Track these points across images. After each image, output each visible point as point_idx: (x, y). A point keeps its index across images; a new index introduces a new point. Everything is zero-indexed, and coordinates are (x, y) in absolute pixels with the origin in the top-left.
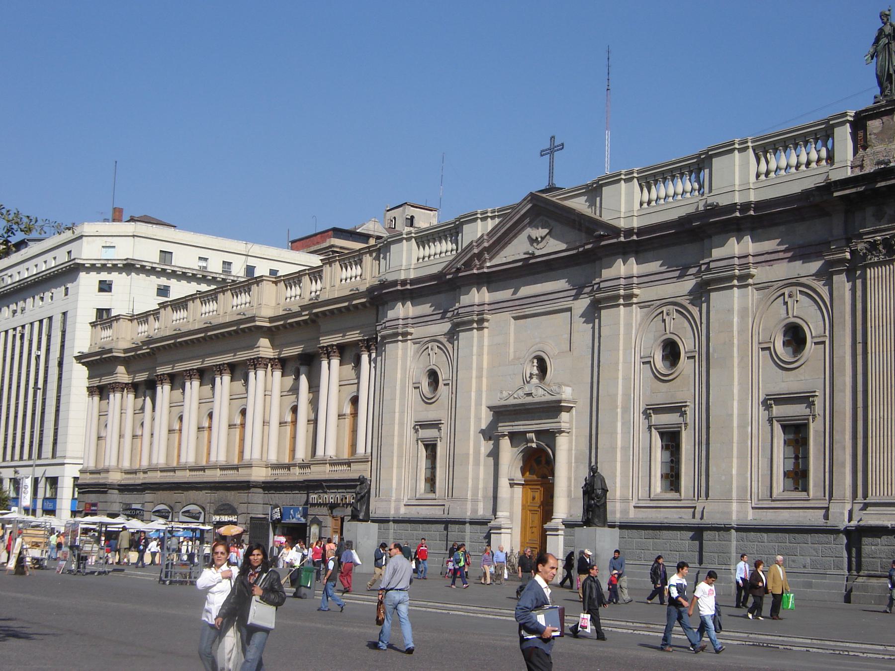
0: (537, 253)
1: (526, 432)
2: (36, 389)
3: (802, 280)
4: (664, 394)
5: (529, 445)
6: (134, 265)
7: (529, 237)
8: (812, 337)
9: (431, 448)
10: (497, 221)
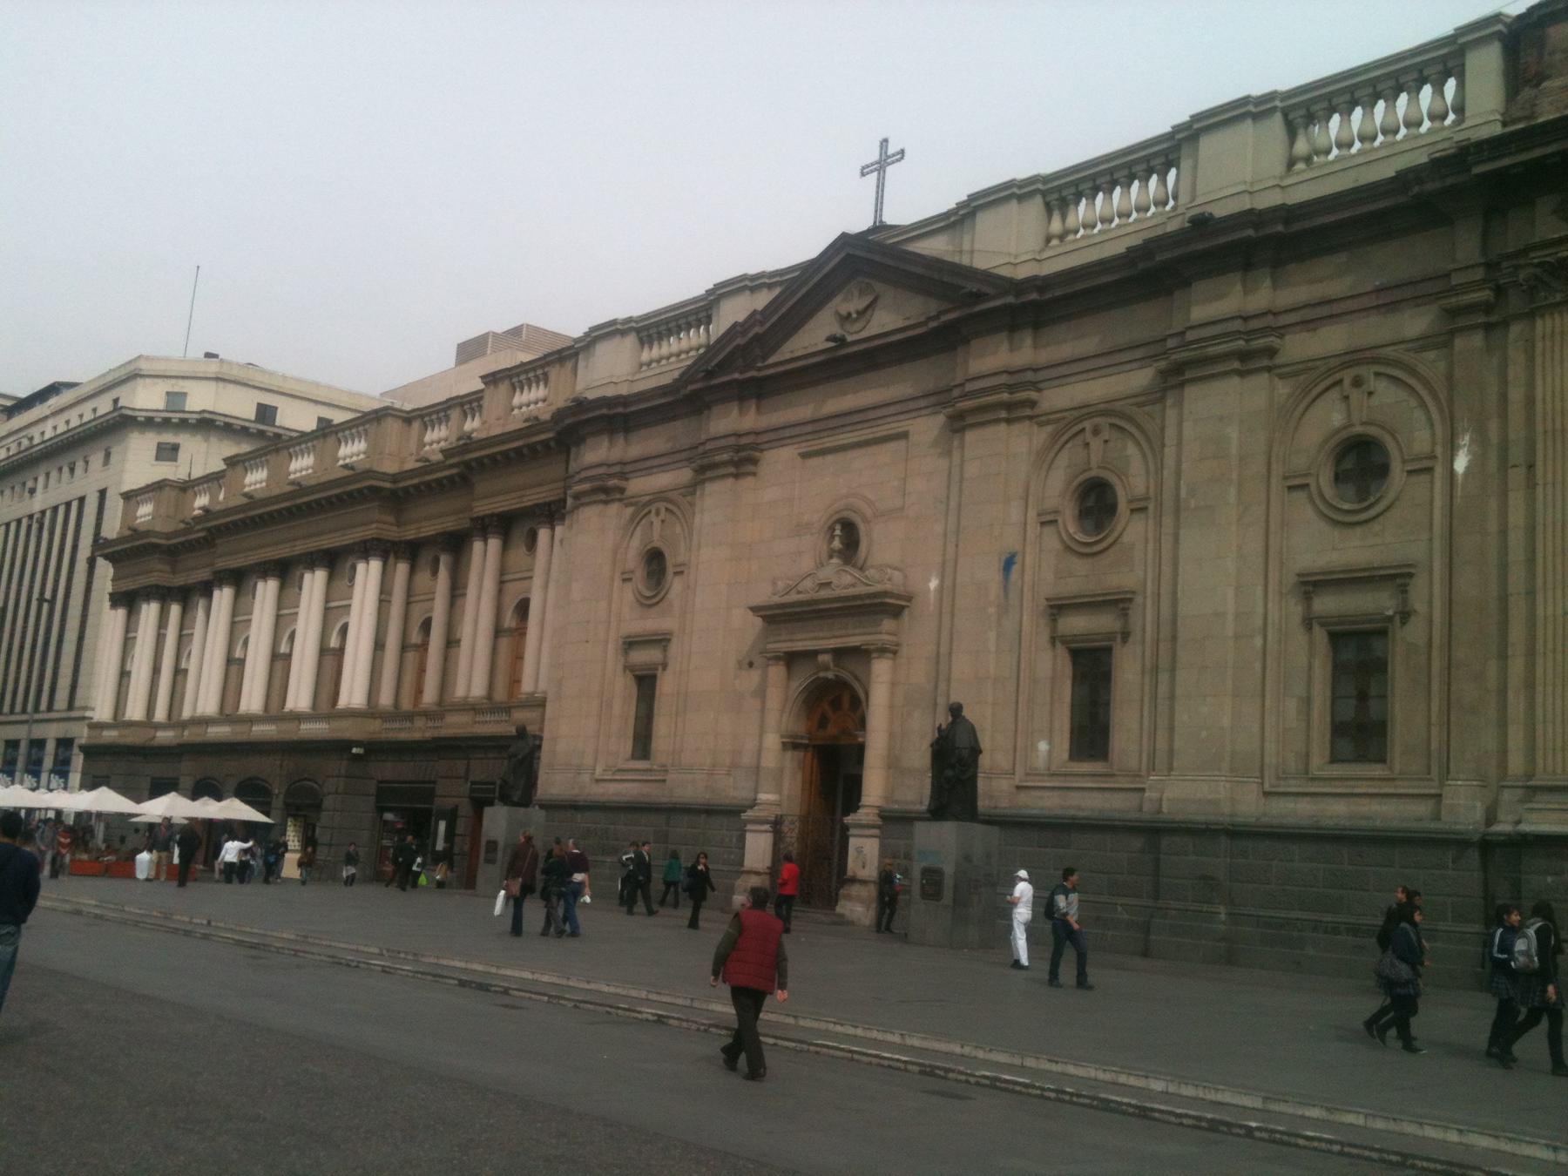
0: (849, 338)
1: (815, 653)
2: (41, 600)
3: (1388, 351)
4: (1081, 578)
5: (822, 674)
6: (213, 421)
7: (838, 314)
8: (1404, 462)
9: (646, 683)
10: (777, 291)
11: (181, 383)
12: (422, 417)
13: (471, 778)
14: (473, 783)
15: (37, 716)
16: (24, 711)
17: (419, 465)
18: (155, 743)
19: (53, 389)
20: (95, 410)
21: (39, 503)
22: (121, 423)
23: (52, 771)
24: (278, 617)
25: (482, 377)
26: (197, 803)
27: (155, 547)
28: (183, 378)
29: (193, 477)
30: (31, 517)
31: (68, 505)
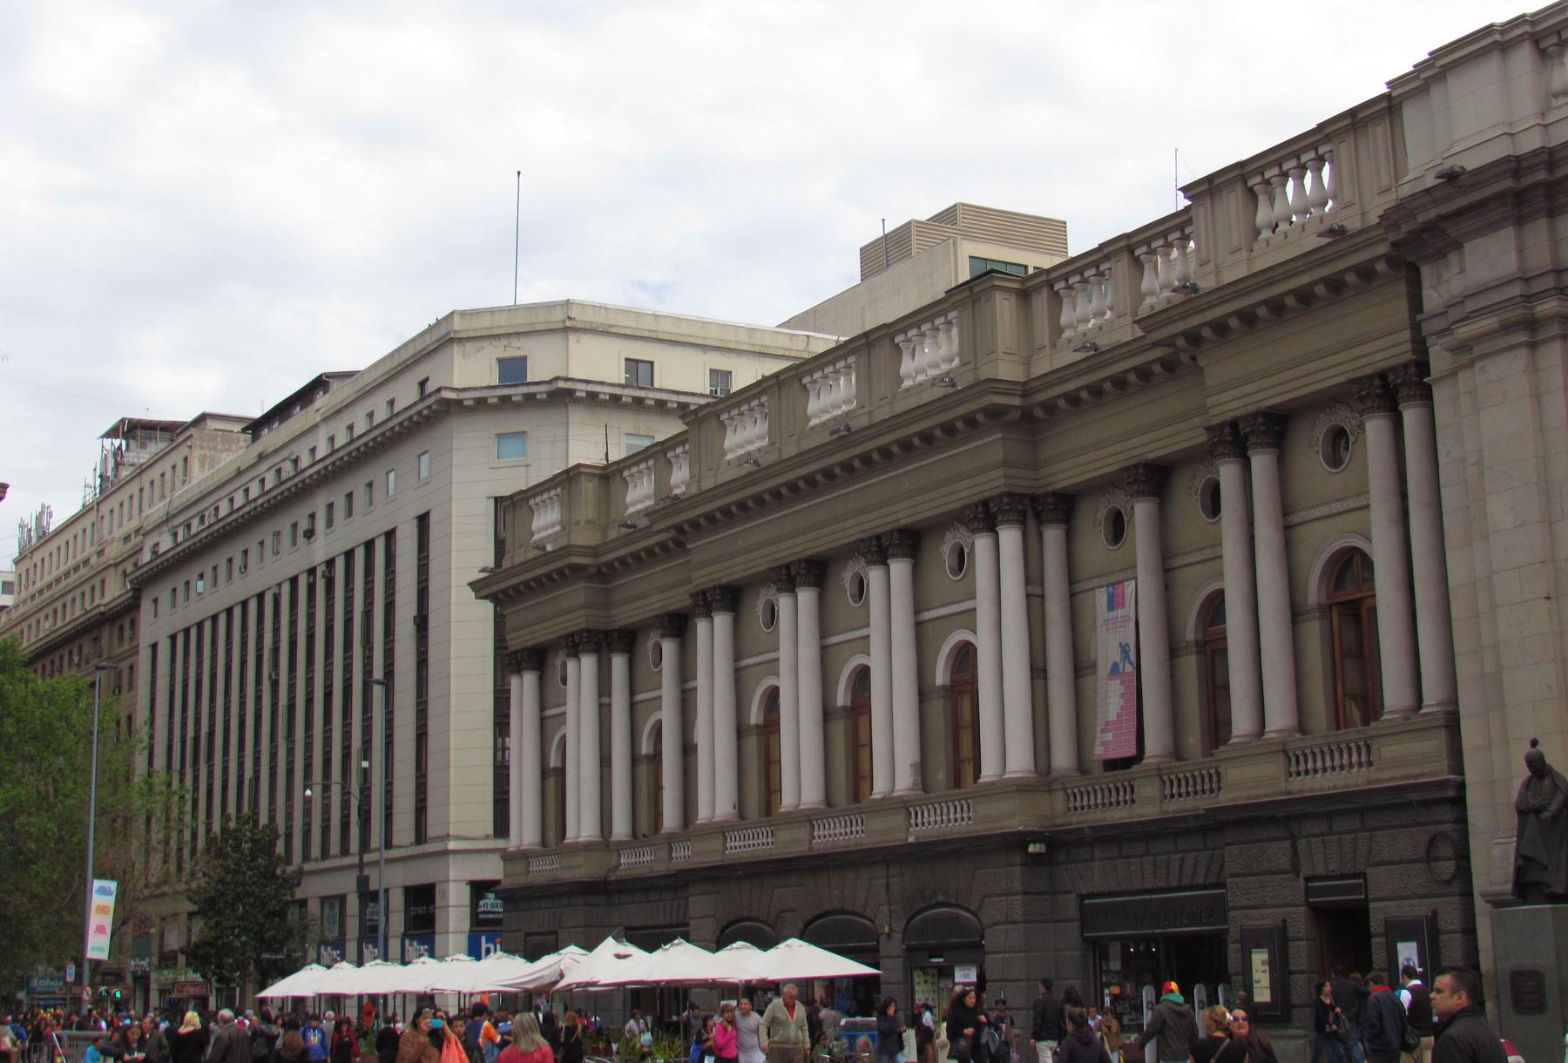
11: (515, 342)
12: (1164, 235)
13: (1306, 870)
14: (1308, 879)
15: (308, 867)
16: (325, 854)
17: (1081, 355)
18: (622, 873)
19: (320, 384)
20: (391, 403)
21: (321, 549)
22: (438, 412)
23: (404, 936)
24: (543, 721)
25: (1185, 189)
26: (723, 954)
27: (577, 569)
28: (518, 334)
29: (613, 457)
30: (312, 571)
31: (187, 631)
